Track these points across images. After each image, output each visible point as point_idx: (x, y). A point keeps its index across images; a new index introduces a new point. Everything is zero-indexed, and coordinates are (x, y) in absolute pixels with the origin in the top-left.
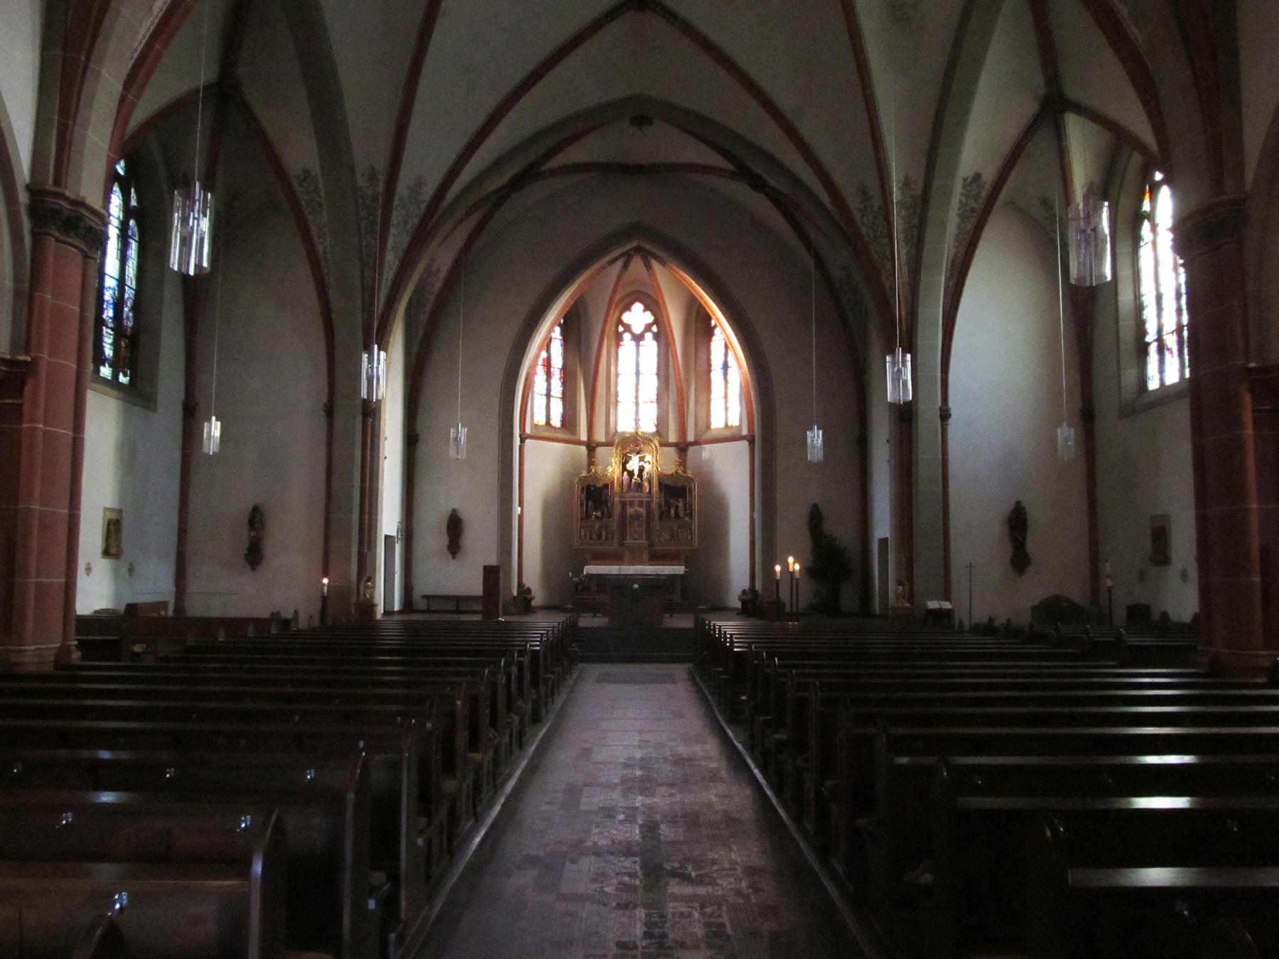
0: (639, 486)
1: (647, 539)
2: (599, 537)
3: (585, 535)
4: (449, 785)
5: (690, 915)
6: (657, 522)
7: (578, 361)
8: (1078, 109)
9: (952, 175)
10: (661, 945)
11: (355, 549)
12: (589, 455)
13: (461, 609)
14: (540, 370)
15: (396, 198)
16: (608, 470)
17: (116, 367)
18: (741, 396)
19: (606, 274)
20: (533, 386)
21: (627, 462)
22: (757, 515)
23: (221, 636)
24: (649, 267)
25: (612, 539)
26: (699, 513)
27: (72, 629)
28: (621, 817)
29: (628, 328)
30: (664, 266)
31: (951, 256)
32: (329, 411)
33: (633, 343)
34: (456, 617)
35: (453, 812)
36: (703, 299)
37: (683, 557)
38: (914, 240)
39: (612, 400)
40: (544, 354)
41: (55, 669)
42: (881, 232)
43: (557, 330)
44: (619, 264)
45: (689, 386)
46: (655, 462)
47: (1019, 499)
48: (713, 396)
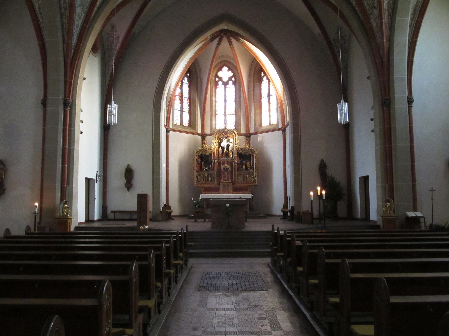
0: (227, 154)
2: (208, 179)
6: (236, 172)
7: (196, 94)
11: (58, 185)
12: (202, 140)
16: (211, 146)
18: (277, 109)
21: (221, 143)
24: (230, 43)
25: (214, 181)
26: (258, 168)
29: (220, 79)
30: (239, 42)
32: (44, 103)
33: (223, 86)
39: (213, 113)
44: (216, 41)
46: (235, 142)
48: (263, 110)
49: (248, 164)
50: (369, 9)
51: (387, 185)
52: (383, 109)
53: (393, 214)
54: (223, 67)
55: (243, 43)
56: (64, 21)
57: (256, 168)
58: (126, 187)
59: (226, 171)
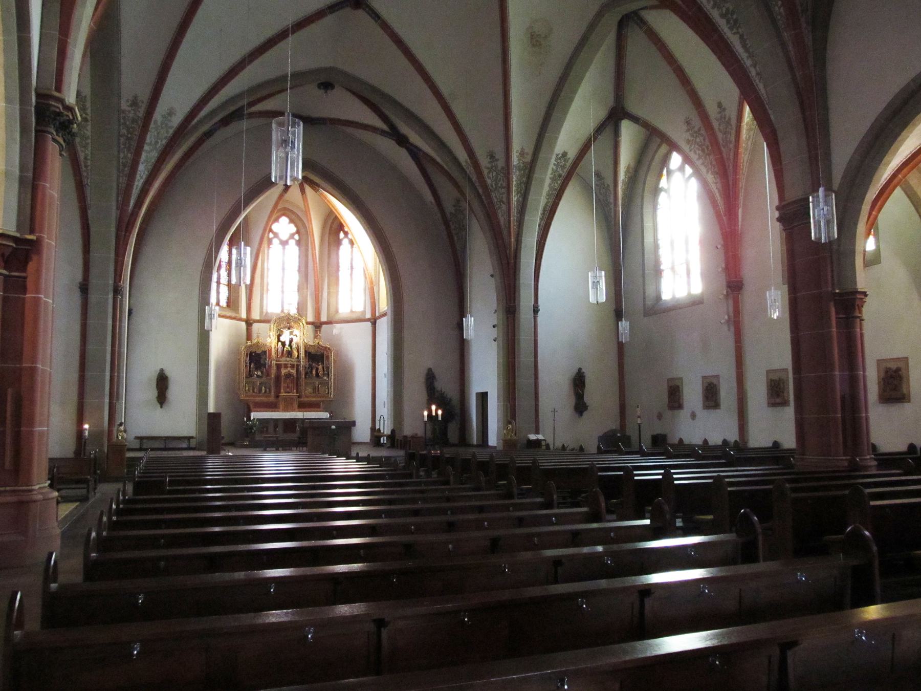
0: (290, 353)
1: (297, 393)
2: (260, 390)
3: (249, 390)
6: (304, 379)
8: (635, 119)
12: (247, 329)
26: (334, 375)
32: (84, 288)
33: (281, 247)
34: (165, 454)
36: (342, 219)
38: (522, 192)
39: (265, 288)
42: (501, 184)
45: (323, 280)
46: (302, 335)
47: (581, 367)
49: (320, 369)
50: (497, 202)
51: (508, 404)
52: (508, 318)
53: (514, 437)
55: (322, 194)
56: (121, 180)
58: (158, 402)
59: (288, 378)
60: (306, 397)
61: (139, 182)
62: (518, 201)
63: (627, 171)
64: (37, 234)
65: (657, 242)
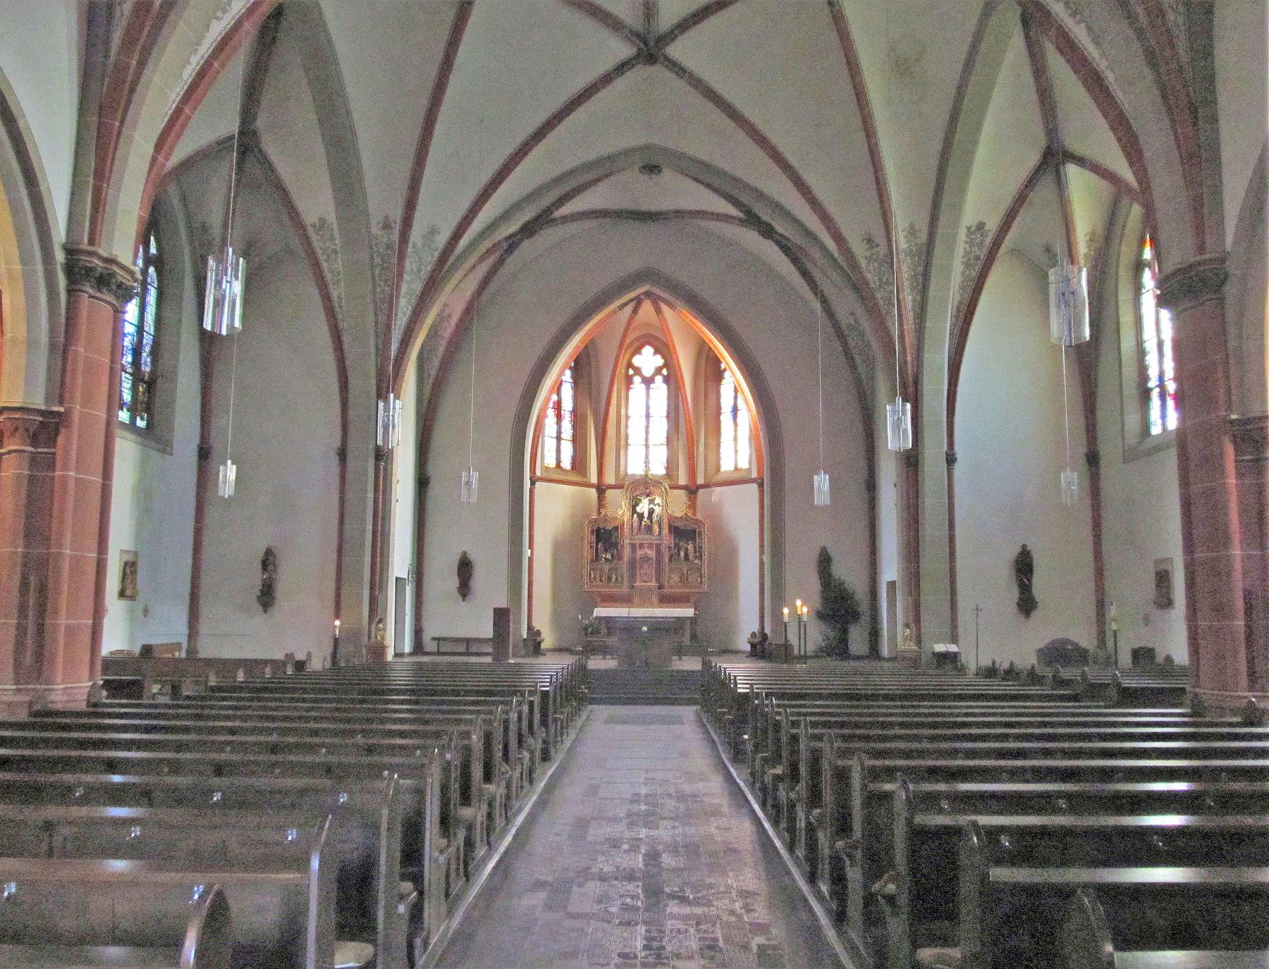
0: (649, 529)
2: (609, 578)
3: (595, 579)
4: (466, 812)
5: (686, 931)
8: (1081, 161)
9: (956, 222)
10: (659, 956)
12: (599, 497)
13: (470, 651)
14: (551, 413)
15: (410, 245)
17: (133, 411)
18: (750, 440)
19: (616, 315)
20: (544, 429)
21: (637, 505)
22: (766, 558)
23: (241, 676)
24: (659, 311)
25: (622, 582)
27: (99, 667)
28: (626, 847)
29: (638, 371)
31: (956, 301)
32: (343, 455)
33: (643, 386)
35: (469, 844)
37: (693, 599)
38: (920, 287)
39: (623, 442)
40: (555, 398)
41: (88, 706)
43: (568, 373)
44: (629, 309)
46: (664, 504)
54: (642, 347)
57: (705, 557)
60: (670, 587)
61: (400, 322)
62: (914, 300)
63: (1092, 239)
64: (66, 405)
65: (1142, 345)
